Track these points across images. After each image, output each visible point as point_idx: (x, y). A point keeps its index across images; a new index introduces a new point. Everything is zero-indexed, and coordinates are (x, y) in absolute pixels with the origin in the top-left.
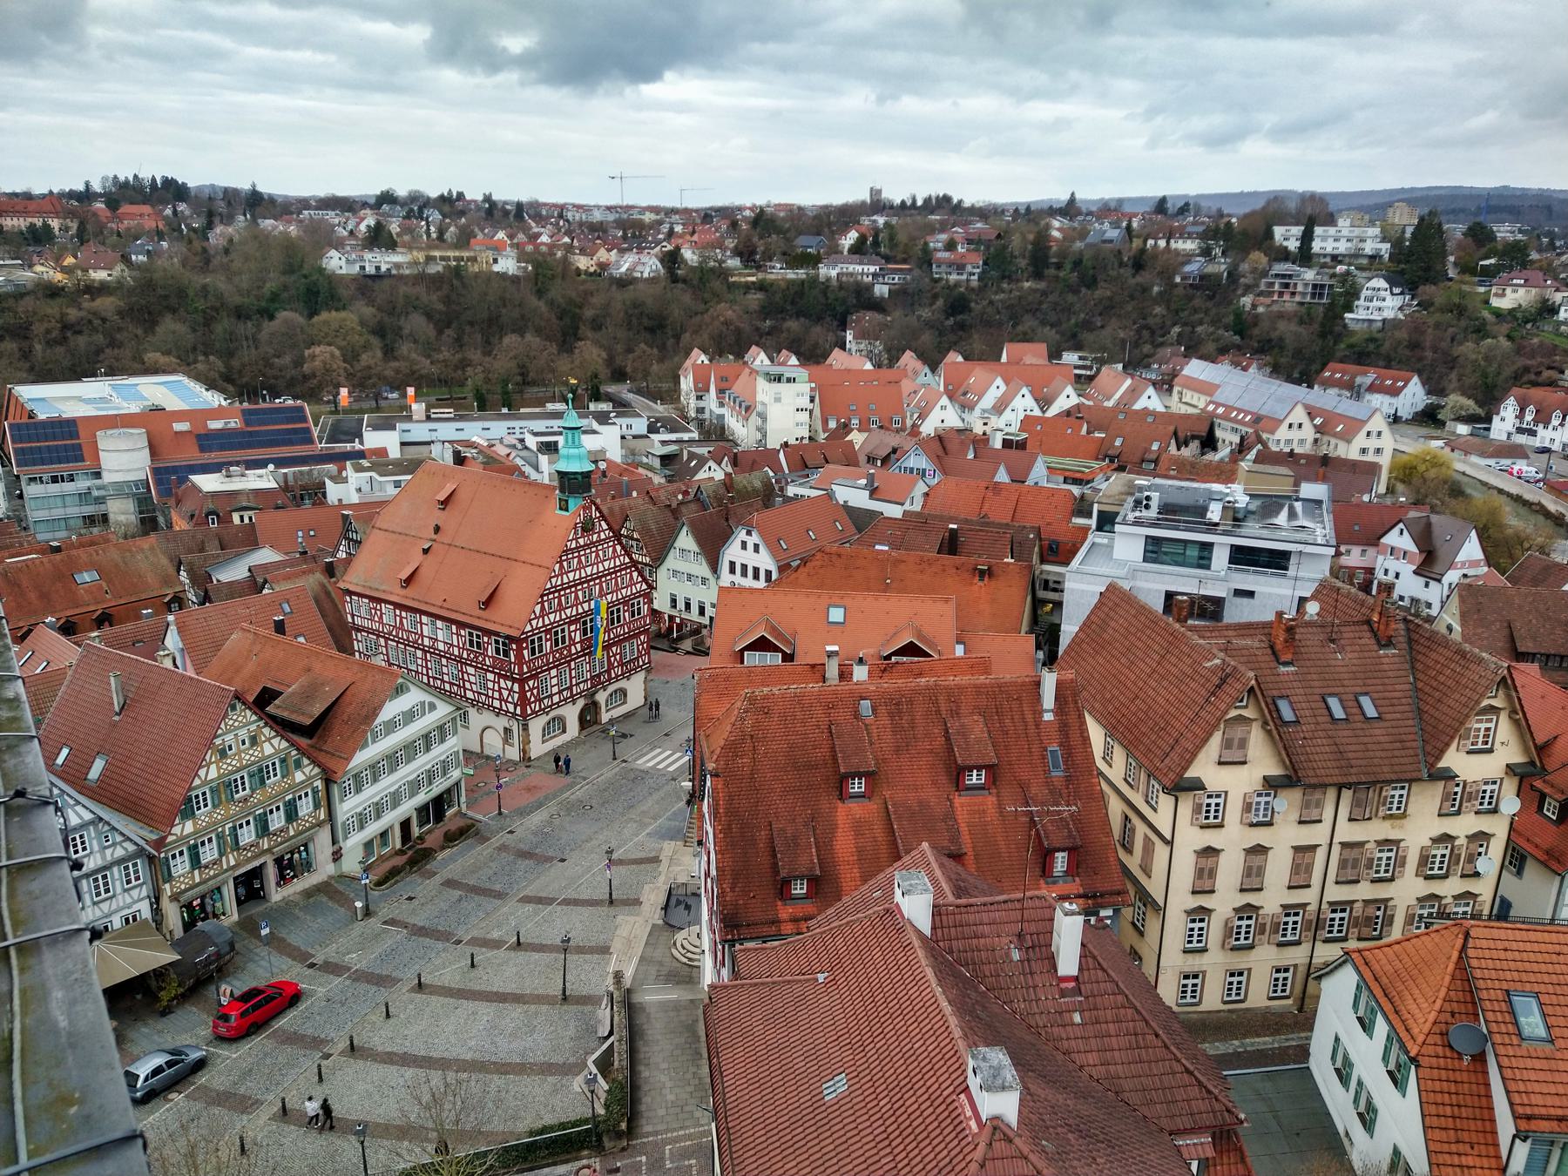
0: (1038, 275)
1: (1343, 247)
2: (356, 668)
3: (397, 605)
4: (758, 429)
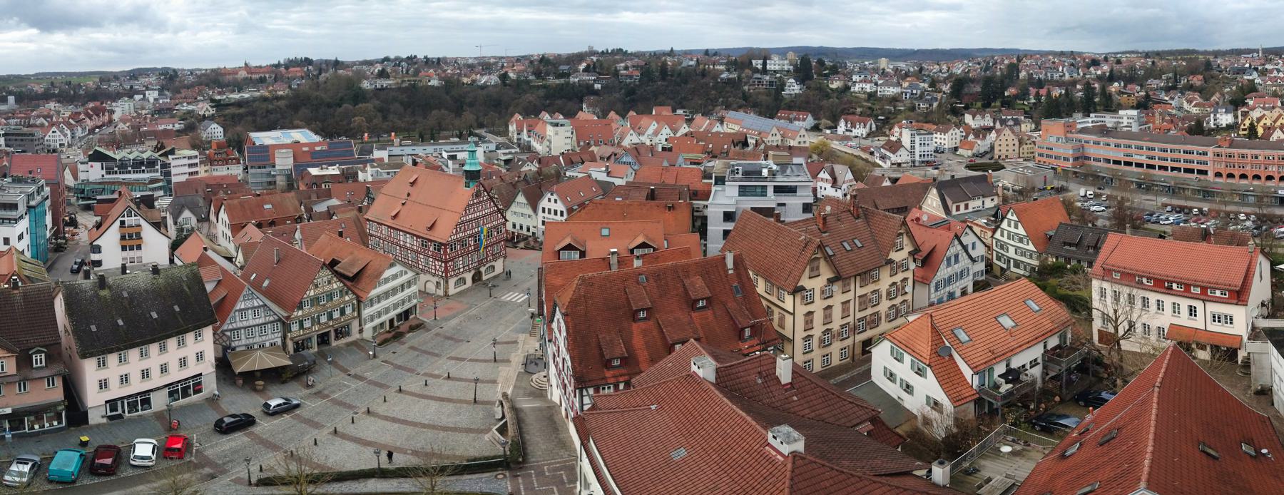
0: (663, 79)
1: (777, 68)
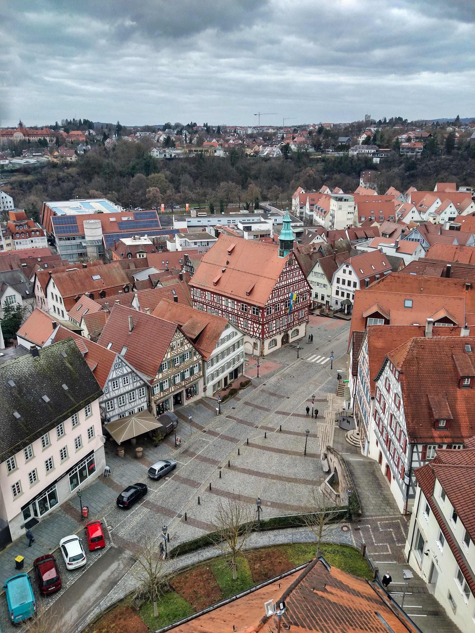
0: (448, 152)
2: (210, 317)
3: (212, 293)
4: (330, 221)
